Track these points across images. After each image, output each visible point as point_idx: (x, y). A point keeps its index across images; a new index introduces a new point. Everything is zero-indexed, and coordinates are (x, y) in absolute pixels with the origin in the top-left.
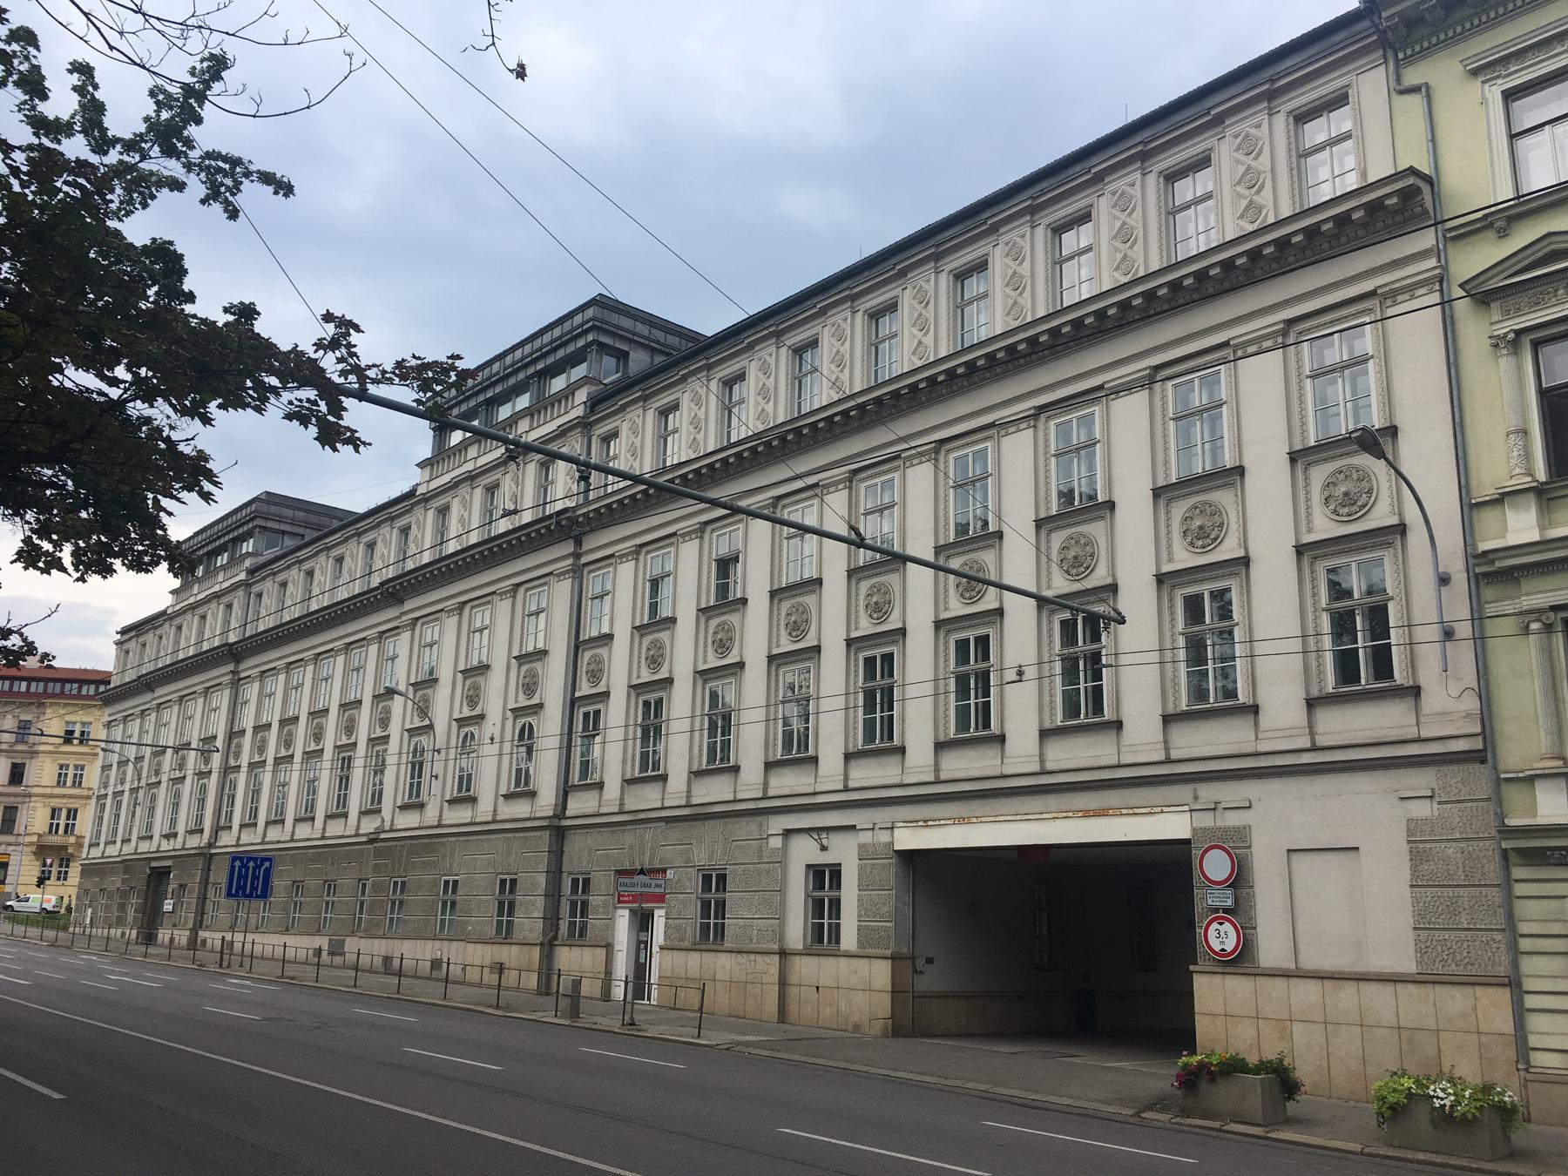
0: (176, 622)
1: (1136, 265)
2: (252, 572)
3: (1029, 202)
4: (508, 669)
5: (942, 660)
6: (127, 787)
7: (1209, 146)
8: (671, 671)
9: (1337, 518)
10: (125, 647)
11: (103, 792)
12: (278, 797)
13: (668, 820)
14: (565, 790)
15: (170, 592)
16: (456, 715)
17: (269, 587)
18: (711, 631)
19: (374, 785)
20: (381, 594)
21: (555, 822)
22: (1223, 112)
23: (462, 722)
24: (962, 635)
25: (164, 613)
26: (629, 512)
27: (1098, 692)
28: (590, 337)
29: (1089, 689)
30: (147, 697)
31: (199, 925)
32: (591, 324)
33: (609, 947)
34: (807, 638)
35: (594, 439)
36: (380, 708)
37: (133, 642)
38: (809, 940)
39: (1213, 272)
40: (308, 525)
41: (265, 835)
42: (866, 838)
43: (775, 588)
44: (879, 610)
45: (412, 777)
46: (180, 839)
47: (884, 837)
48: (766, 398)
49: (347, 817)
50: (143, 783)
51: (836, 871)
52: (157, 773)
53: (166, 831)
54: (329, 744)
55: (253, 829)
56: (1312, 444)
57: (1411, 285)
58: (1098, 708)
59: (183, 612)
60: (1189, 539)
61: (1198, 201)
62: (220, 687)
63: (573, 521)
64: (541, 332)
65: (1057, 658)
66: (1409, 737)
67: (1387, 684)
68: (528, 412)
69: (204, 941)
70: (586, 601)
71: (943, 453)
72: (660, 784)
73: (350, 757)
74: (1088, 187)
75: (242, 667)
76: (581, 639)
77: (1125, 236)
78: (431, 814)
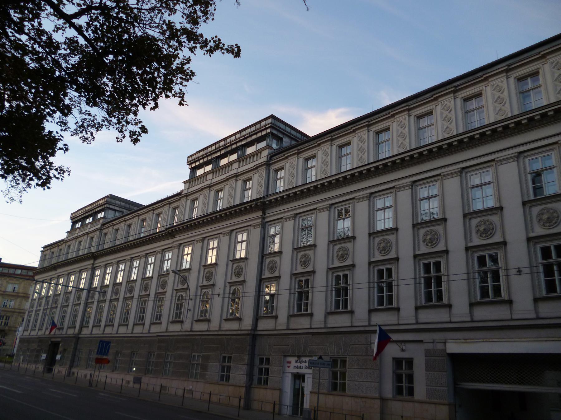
0: (68, 244)
1: (452, 131)
2: (103, 225)
3: (506, 67)
4: (227, 265)
5: (471, 264)
6: (42, 308)
7: (350, 139)
8: (314, 268)
9: (381, 254)
10: (45, 253)
11: (31, 309)
12: (87, 317)
13: (313, 334)
14: (257, 318)
15: (67, 232)
16: (200, 284)
17: (110, 230)
18: (336, 250)
19: (157, 312)
20: (165, 233)
21: (252, 332)
22: (545, 54)
23: (203, 287)
24: (380, 268)
25: (63, 240)
26: (285, 202)
27: (346, 300)
28: (269, 131)
29: (344, 300)
30: (53, 273)
31: (71, 367)
32: (270, 125)
33: (281, 390)
34: (275, 273)
35: (271, 171)
36: (66, 296)
37: (48, 252)
38: (395, 394)
39: (291, 195)
40: (125, 208)
41: (104, 331)
42: (430, 346)
43: (372, 232)
44: (343, 257)
45: (177, 309)
46: (65, 330)
47: (440, 346)
48: (292, 176)
49: (113, 326)
50: (49, 307)
51: (410, 362)
52: (56, 303)
53: (70, 325)
54: (136, 294)
55: (98, 328)
56: (336, 239)
57: (404, 186)
58: (390, 302)
59: (72, 239)
60: (425, 243)
61: (386, 141)
62: (87, 270)
63: (264, 203)
64: (207, 148)
65: (540, 265)
66: (204, 330)
67: (499, 299)
68: (212, 172)
69: (73, 373)
70: (267, 237)
71: (372, 198)
72: (309, 317)
73: (145, 301)
74: (432, 102)
75: (97, 262)
76: (265, 253)
77: (325, 163)
78: (187, 326)
